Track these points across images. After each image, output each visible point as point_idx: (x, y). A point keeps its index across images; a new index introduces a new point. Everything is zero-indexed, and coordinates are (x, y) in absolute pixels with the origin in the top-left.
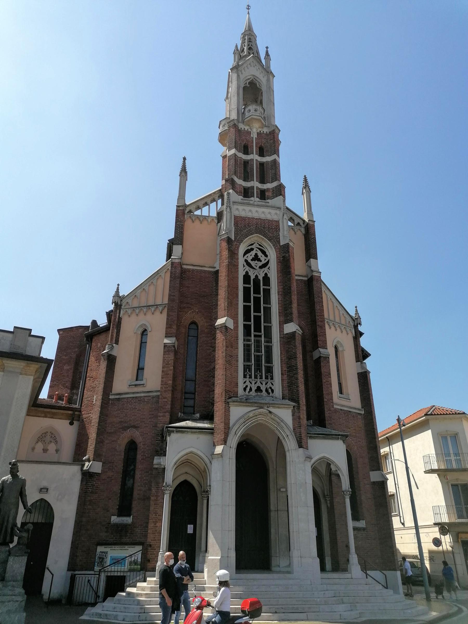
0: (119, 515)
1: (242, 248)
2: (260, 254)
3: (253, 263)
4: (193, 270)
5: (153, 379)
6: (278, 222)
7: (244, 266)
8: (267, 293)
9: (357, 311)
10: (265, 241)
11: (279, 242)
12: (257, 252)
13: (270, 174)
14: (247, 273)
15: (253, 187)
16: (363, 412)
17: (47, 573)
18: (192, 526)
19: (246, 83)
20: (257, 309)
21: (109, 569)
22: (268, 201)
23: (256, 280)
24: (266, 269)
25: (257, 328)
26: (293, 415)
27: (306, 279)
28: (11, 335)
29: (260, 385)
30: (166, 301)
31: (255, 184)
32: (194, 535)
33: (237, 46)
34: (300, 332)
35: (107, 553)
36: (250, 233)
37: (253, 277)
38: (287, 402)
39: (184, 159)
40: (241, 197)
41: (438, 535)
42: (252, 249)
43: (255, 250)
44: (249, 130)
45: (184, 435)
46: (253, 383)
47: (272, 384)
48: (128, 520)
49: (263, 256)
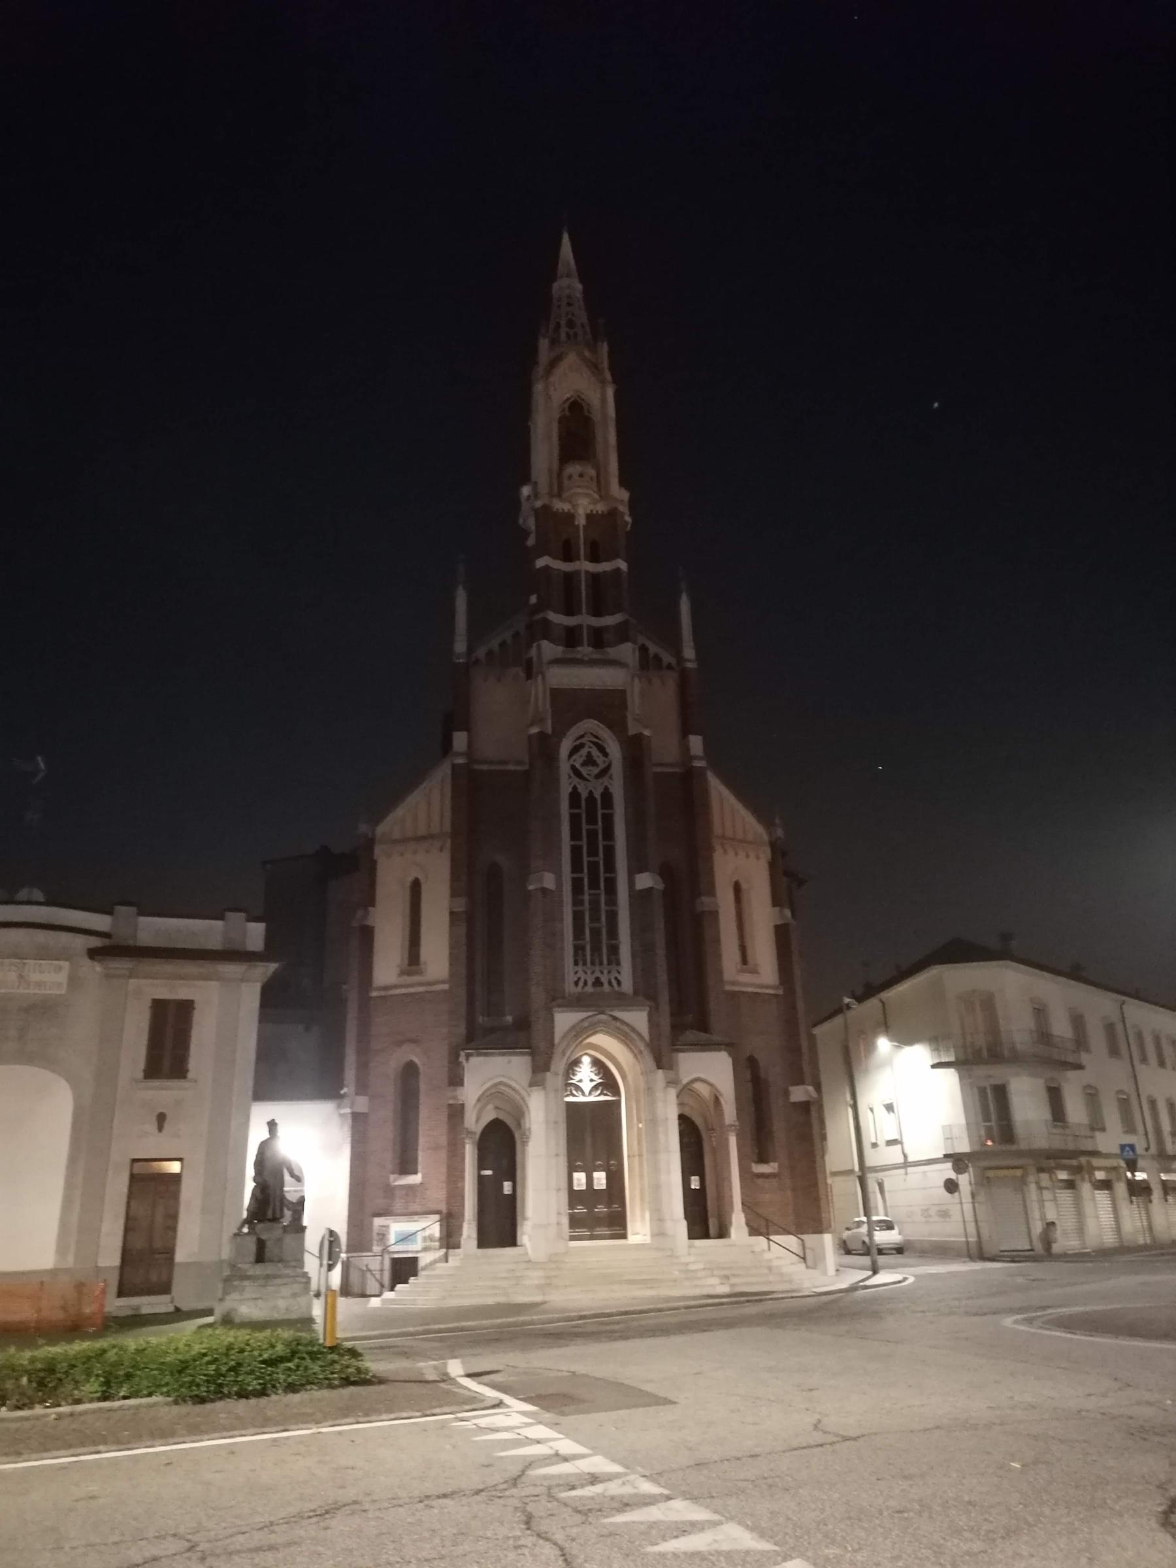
1: (566, 746)
2: (595, 752)
3: (584, 771)
6: (623, 692)
7: (570, 777)
8: (608, 821)
11: (625, 728)
14: (575, 788)
15: (580, 627)
16: (780, 992)
20: (593, 852)
21: (392, 1249)
22: (609, 650)
23: (591, 798)
24: (605, 781)
25: (594, 884)
26: (649, 1021)
30: (447, 827)
31: (585, 620)
32: (513, 1198)
34: (660, 886)
35: (387, 1227)
37: (584, 795)
40: (560, 649)
41: (952, 1175)
42: (582, 746)
45: (488, 1059)
46: (589, 972)
48: (415, 1179)
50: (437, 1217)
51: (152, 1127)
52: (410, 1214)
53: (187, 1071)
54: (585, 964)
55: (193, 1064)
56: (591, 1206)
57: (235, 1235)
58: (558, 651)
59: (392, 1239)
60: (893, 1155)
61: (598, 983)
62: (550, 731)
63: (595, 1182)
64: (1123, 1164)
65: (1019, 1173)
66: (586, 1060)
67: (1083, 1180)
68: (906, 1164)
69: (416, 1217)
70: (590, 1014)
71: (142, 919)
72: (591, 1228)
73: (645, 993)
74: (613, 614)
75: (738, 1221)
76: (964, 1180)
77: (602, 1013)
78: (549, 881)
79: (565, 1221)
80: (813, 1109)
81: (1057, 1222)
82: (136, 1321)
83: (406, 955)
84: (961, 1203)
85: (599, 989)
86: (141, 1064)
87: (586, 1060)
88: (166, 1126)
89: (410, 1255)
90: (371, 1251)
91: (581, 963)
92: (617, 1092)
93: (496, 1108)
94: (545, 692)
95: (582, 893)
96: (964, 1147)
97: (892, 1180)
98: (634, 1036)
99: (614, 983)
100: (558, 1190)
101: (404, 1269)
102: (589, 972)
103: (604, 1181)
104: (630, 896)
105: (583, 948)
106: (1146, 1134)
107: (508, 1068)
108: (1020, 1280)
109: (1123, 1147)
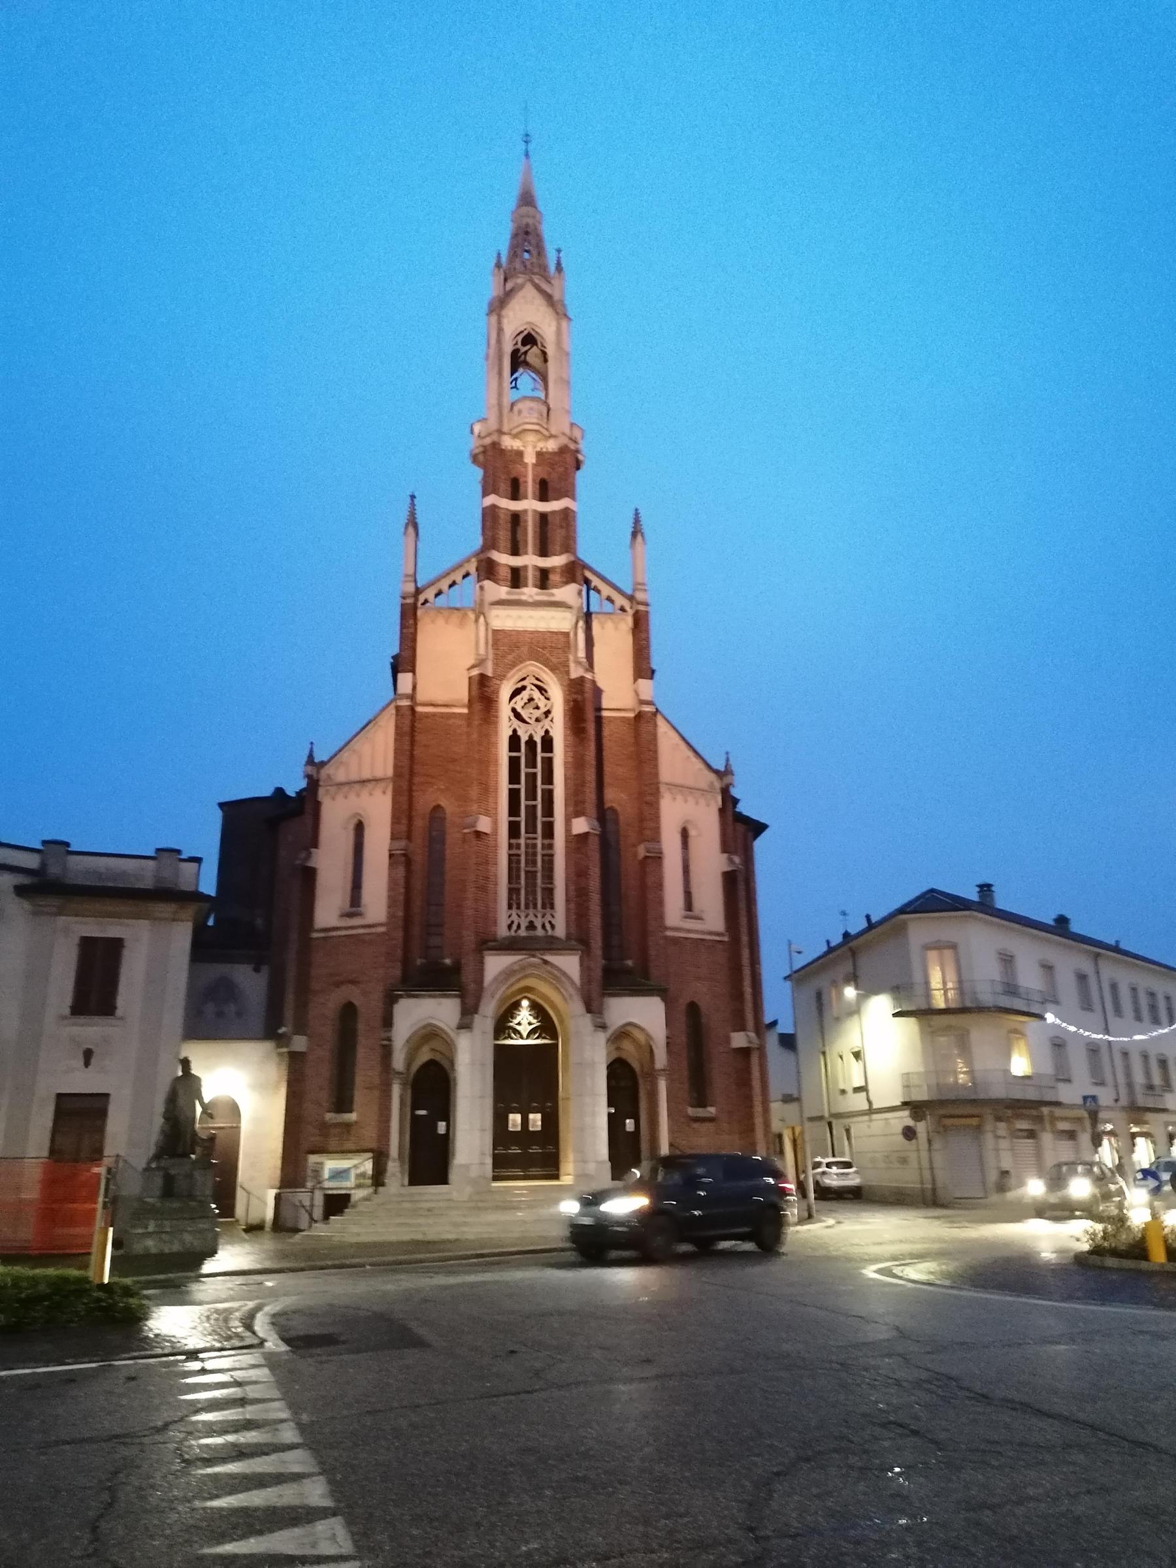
2: (536, 694)
3: (524, 714)
4: (434, 715)
5: (377, 903)
9: (728, 760)
11: (568, 673)
13: (557, 535)
14: (515, 731)
17: (240, 1194)
18: (444, 1123)
21: (327, 1184)
22: (554, 591)
23: (531, 743)
24: (546, 723)
26: (581, 965)
27: (632, 715)
28: (151, 863)
29: (533, 919)
30: (390, 772)
31: (530, 560)
33: (499, 255)
35: (322, 1163)
37: (524, 738)
39: (413, 497)
41: (911, 1123)
42: (524, 688)
48: (353, 1117)
49: (542, 698)
50: (370, 1155)
51: (82, 1063)
52: (344, 1152)
53: (115, 1008)
54: (518, 908)
55: (121, 1001)
56: (525, 1146)
57: (145, 1170)
58: (503, 592)
59: (326, 1175)
60: (858, 1102)
61: (531, 926)
62: (490, 674)
63: (531, 1123)
64: (1086, 1115)
65: (974, 1122)
66: (525, 1003)
67: (1044, 1130)
68: (871, 1111)
69: (350, 1155)
72: (524, 1169)
73: (578, 940)
76: (921, 1128)
77: (534, 956)
79: (489, 1161)
80: (755, 1059)
81: (1012, 1171)
82: (465, 1224)
83: (349, 899)
84: (918, 1150)
85: (532, 933)
86: (68, 1000)
87: (525, 1003)
88: (93, 1061)
89: (343, 1192)
90: (304, 1187)
91: (515, 906)
92: (554, 1036)
93: (433, 1050)
96: (921, 1095)
97: (859, 1127)
98: (563, 979)
99: (548, 926)
100: (483, 1130)
101: (337, 1204)
103: (539, 1123)
104: (567, 841)
105: (518, 891)
106: (1116, 1086)
107: (440, 1010)
109: (1085, 1098)
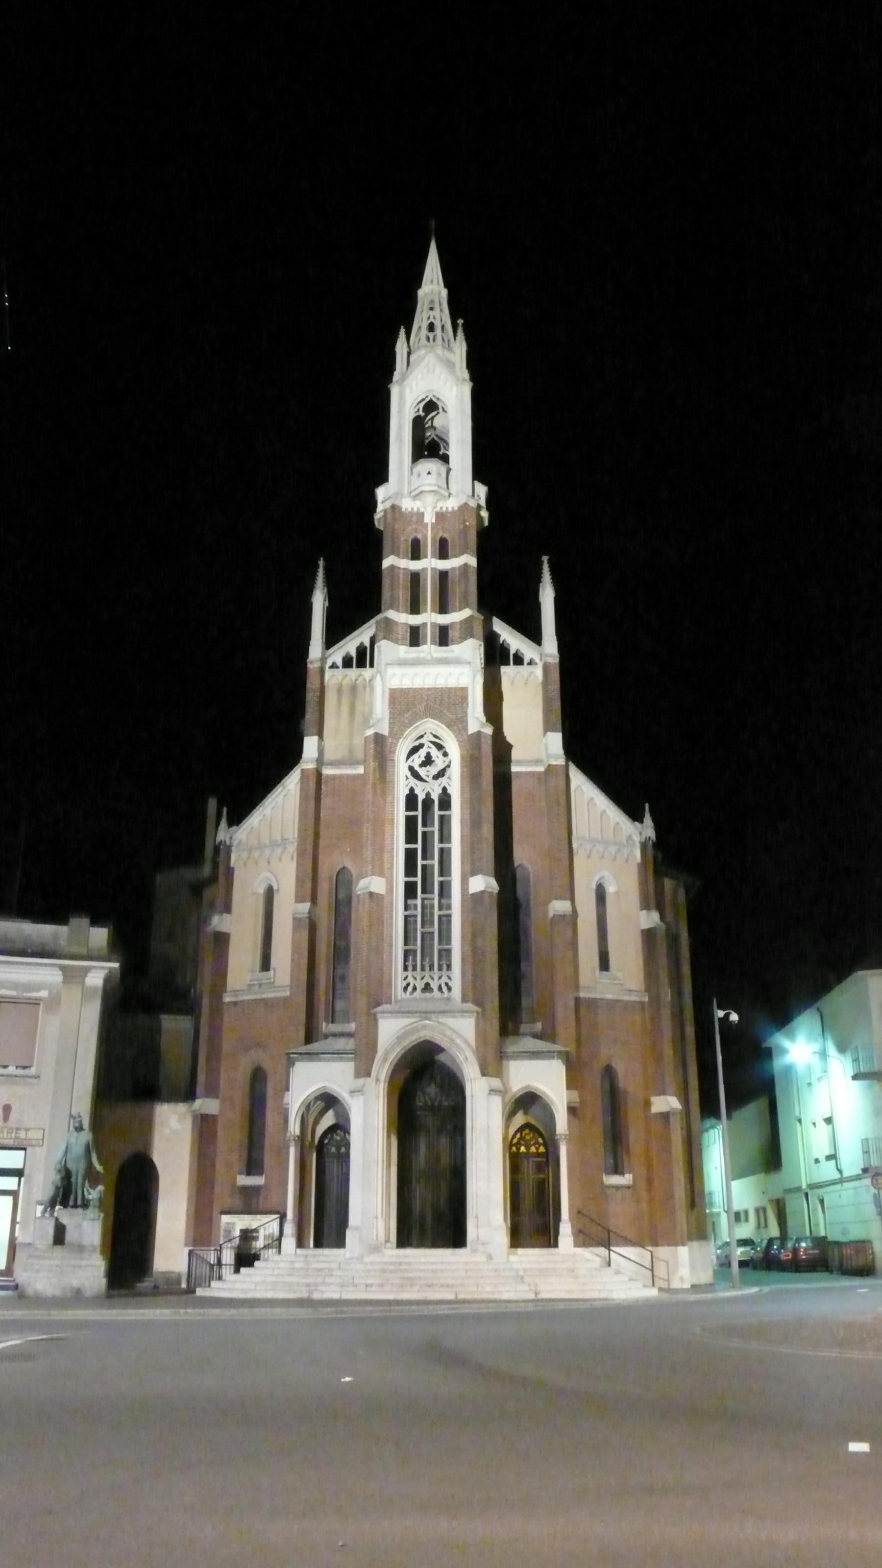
0: (249, 1173)
2: (434, 752)
3: (422, 772)
7: (407, 778)
10: (442, 729)
11: (466, 730)
12: (429, 750)
14: (412, 790)
19: (418, 410)
23: (428, 802)
24: (443, 781)
31: (429, 618)
36: (416, 718)
37: (421, 797)
38: (470, 1006)
42: (421, 746)
43: (426, 746)
44: (422, 510)
46: (418, 978)
47: (450, 978)
62: (385, 731)
70: (413, 1020)
71: (92, 929)
74: (460, 610)
75: (566, 1229)
78: (376, 884)
85: (427, 995)
94: (383, 693)
95: (416, 897)
99: (444, 988)
102: (418, 978)
108: (323, 1288)
